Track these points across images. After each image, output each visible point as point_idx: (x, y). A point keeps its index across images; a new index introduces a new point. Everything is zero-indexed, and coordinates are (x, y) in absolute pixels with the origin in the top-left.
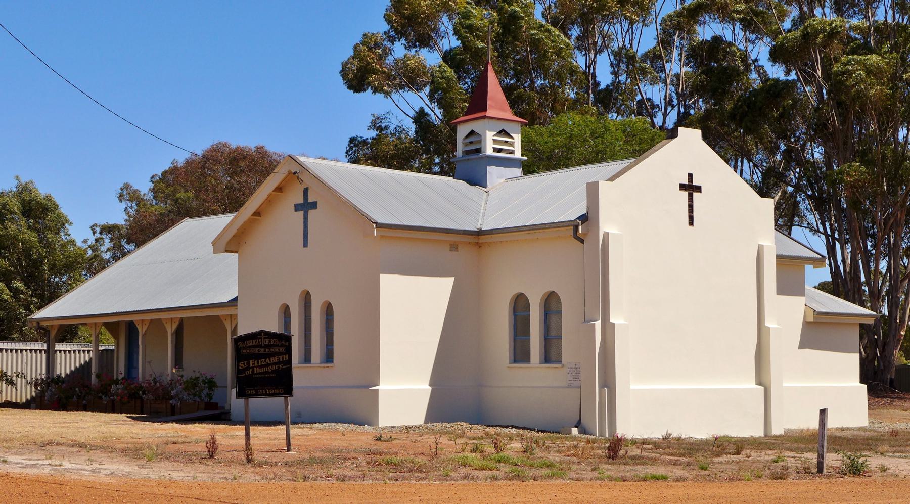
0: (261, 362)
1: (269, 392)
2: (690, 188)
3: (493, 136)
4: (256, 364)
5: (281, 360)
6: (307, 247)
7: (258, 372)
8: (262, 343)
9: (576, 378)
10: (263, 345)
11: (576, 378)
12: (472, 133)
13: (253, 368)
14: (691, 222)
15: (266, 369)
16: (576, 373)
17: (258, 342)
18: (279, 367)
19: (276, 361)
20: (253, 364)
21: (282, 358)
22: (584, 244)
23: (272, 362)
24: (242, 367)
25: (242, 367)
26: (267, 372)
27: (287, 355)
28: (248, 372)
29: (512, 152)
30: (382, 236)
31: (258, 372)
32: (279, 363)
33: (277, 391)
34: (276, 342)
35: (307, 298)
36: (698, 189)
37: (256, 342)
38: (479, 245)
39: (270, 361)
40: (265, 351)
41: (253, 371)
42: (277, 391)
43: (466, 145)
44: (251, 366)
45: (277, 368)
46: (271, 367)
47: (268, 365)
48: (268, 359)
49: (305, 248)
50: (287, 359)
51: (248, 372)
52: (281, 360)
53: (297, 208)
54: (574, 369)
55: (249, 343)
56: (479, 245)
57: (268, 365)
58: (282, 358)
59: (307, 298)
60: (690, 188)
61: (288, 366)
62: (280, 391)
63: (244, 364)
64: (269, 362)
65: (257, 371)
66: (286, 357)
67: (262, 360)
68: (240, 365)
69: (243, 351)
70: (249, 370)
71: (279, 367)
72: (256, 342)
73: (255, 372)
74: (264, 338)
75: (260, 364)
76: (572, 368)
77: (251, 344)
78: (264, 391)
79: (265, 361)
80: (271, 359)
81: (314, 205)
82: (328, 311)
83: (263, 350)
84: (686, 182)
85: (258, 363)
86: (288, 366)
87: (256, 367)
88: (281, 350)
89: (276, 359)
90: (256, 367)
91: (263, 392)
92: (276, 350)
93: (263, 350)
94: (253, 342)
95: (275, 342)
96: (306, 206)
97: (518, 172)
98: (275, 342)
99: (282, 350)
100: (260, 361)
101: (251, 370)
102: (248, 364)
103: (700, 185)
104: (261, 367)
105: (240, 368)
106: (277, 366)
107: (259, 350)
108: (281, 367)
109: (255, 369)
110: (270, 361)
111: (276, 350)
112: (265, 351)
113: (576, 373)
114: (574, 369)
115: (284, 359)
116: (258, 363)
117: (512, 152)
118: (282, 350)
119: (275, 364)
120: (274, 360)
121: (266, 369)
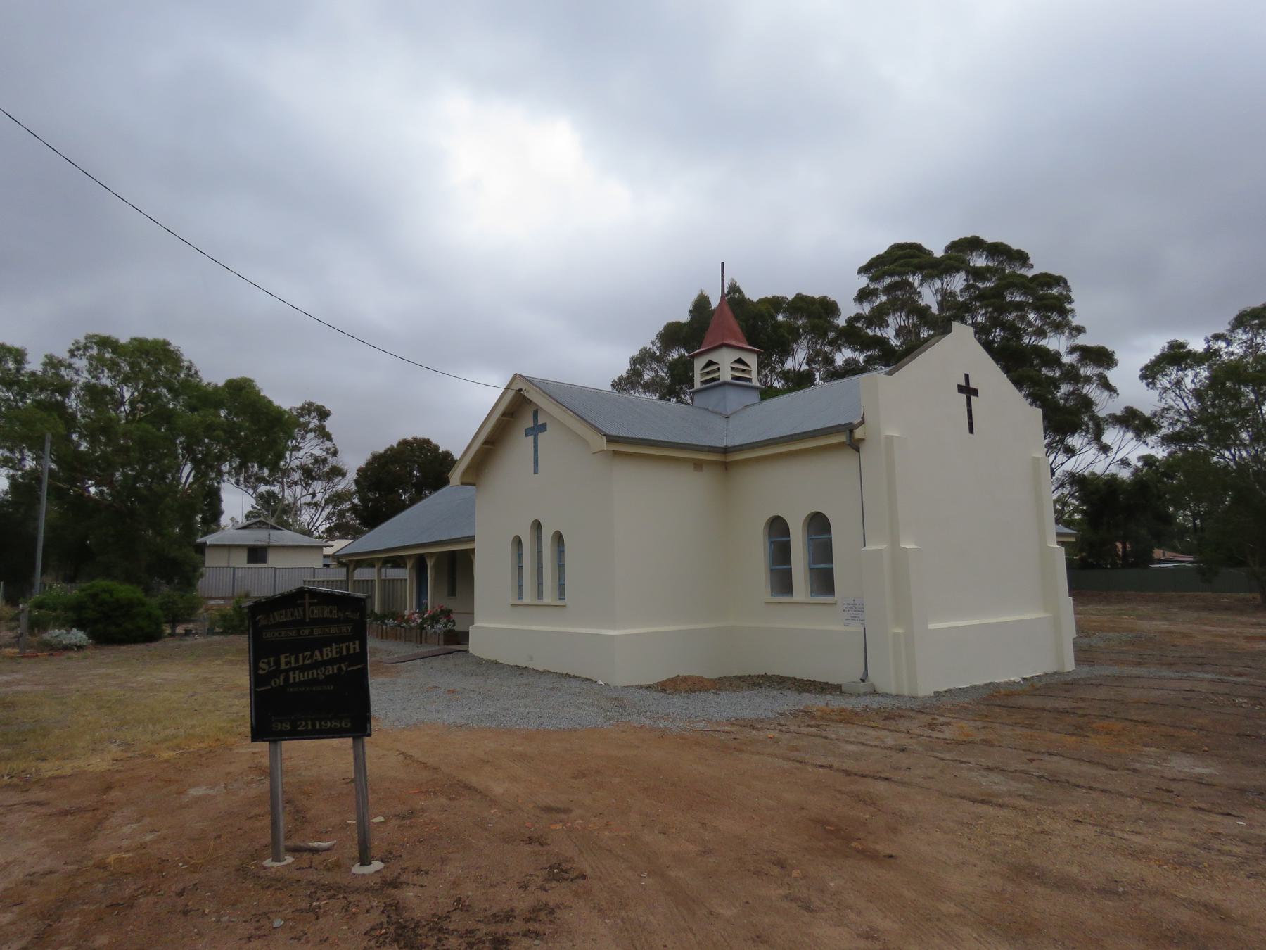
0: (304, 658)
1: (321, 726)
2: (968, 390)
3: (732, 363)
4: (293, 665)
5: (344, 653)
6: (537, 473)
7: (297, 680)
8: (304, 615)
9: (854, 617)
10: (307, 620)
11: (854, 617)
12: (710, 363)
13: (287, 671)
14: (971, 431)
15: (314, 674)
16: (855, 611)
17: (296, 614)
18: (340, 669)
19: (335, 655)
20: (287, 663)
21: (348, 648)
22: (859, 452)
23: (325, 658)
24: (264, 670)
25: (264, 670)
26: (315, 682)
27: (357, 642)
28: (277, 680)
29: (750, 380)
30: (615, 453)
31: (297, 680)
32: (340, 659)
33: (336, 724)
34: (327, 612)
35: (537, 526)
36: (975, 392)
37: (292, 614)
38: (726, 466)
39: (322, 655)
40: (311, 633)
41: (287, 679)
42: (336, 724)
43: (702, 375)
44: (283, 667)
45: (336, 671)
46: (323, 669)
47: (317, 665)
48: (317, 652)
49: (536, 475)
50: (358, 650)
51: (277, 680)
52: (344, 653)
53: (528, 432)
54: (852, 606)
55: (279, 616)
56: (726, 466)
57: (317, 665)
58: (348, 648)
59: (537, 526)
60: (968, 390)
61: (360, 666)
62: (343, 724)
63: (268, 663)
64: (319, 658)
65: (294, 678)
66: (354, 646)
67: (306, 654)
68: (261, 665)
69: (268, 635)
70: (279, 678)
71: (340, 669)
72: (292, 614)
73: (291, 681)
74: (311, 604)
75: (301, 663)
76: (849, 604)
77: (290, 618)
78: (310, 723)
79: (311, 656)
80: (324, 650)
81: (543, 427)
82: (559, 538)
83: (307, 632)
84: (963, 383)
85: (297, 660)
86: (360, 666)
87: (294, 669)
88: (344, 630)
89: (334, 652)
90: (294, 669)
91: (307, 725)
92: (333, 630)
93: (307, 632)
94: (286, 614)
95: (331, 612)
96: (539, 429)
97: (755, 397)
98: (331, 612)
99: (346, 629)
100: (301, 656)
101: (282, 678)
102: (278, 663)
103: (976, 388)
104: (303, 669)
105: (261, 672)
106: (335, 667)
107: (299, 631)
108: (344, 669)
109: (291, 674)
110: (322, 655)
111: (333, 630)
112: (311, 633)
113: (855, 611)
114: (852, 606)
115: (352, 651)
116: (297, 660)
117: (750, 380)
118: (346, 629)
119: (331, 662)
120: (330, 652)
121: (314, 674)
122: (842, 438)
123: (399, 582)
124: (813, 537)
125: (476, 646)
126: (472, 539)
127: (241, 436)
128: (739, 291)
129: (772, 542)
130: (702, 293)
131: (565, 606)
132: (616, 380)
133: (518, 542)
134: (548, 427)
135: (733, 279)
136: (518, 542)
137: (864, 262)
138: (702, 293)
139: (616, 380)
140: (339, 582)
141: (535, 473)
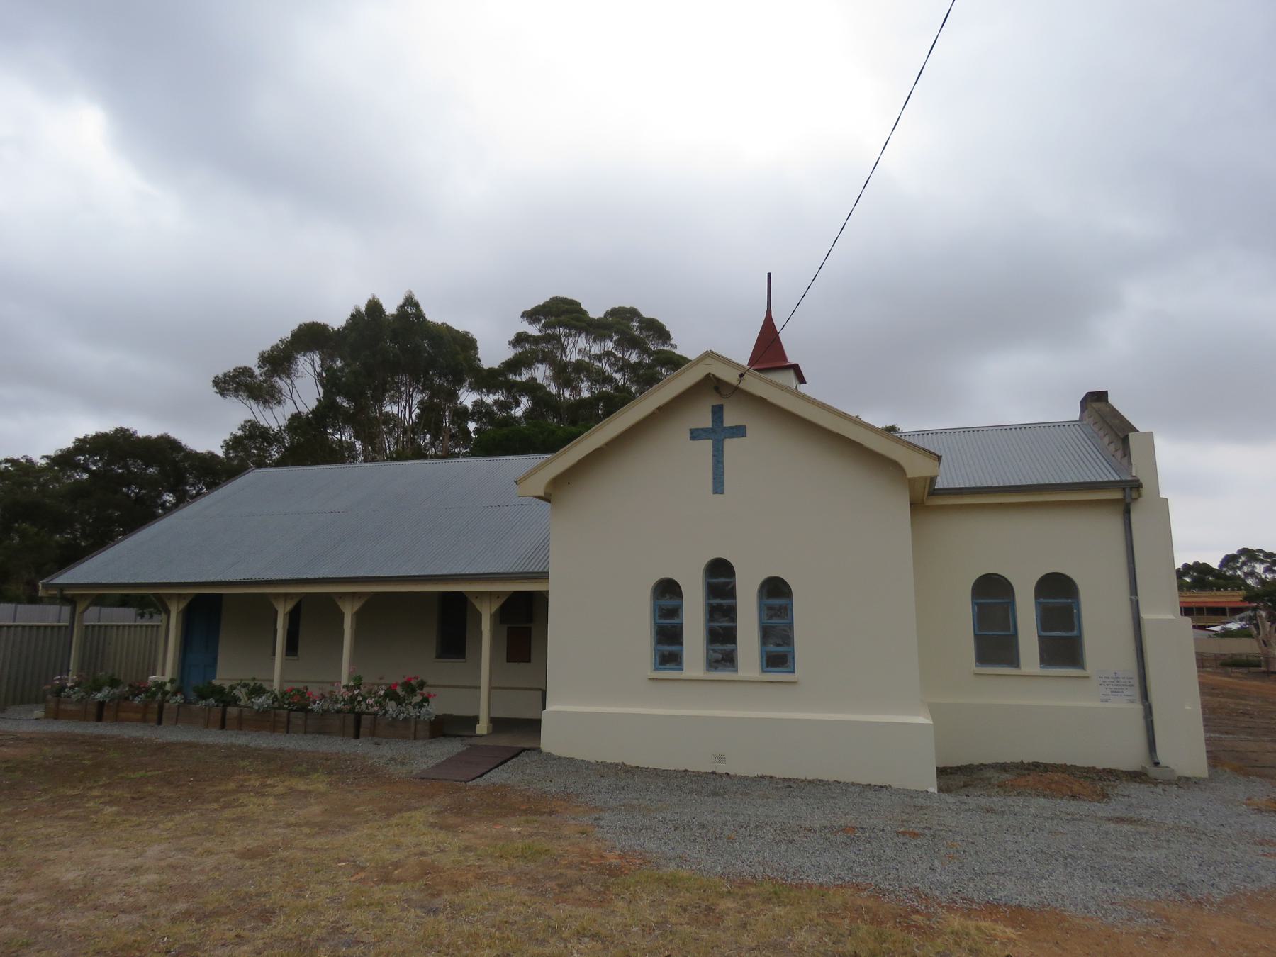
35: (720, 572)
59: (720, 572)
82: (775, 590)
122: (1117, 495)
123: (115, 629)
124: (1042, 600)
125: (551, 740)
126: (544, 576)
127: (342, 358)
128: (417, 305)
129: (977, 604)
130: (374, 298)
131: (794, 683)
132: (221, 376)
133: (668, 590)
134: (748, 432)
135: (411, 292)
136: (668, 590)
137: (529, 307)
138: (374, 298)
139: (221, 376)
140: (20, 629)
141: (715, 492)
